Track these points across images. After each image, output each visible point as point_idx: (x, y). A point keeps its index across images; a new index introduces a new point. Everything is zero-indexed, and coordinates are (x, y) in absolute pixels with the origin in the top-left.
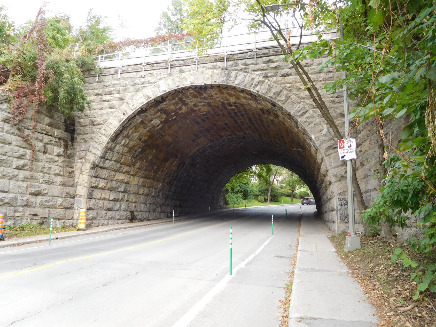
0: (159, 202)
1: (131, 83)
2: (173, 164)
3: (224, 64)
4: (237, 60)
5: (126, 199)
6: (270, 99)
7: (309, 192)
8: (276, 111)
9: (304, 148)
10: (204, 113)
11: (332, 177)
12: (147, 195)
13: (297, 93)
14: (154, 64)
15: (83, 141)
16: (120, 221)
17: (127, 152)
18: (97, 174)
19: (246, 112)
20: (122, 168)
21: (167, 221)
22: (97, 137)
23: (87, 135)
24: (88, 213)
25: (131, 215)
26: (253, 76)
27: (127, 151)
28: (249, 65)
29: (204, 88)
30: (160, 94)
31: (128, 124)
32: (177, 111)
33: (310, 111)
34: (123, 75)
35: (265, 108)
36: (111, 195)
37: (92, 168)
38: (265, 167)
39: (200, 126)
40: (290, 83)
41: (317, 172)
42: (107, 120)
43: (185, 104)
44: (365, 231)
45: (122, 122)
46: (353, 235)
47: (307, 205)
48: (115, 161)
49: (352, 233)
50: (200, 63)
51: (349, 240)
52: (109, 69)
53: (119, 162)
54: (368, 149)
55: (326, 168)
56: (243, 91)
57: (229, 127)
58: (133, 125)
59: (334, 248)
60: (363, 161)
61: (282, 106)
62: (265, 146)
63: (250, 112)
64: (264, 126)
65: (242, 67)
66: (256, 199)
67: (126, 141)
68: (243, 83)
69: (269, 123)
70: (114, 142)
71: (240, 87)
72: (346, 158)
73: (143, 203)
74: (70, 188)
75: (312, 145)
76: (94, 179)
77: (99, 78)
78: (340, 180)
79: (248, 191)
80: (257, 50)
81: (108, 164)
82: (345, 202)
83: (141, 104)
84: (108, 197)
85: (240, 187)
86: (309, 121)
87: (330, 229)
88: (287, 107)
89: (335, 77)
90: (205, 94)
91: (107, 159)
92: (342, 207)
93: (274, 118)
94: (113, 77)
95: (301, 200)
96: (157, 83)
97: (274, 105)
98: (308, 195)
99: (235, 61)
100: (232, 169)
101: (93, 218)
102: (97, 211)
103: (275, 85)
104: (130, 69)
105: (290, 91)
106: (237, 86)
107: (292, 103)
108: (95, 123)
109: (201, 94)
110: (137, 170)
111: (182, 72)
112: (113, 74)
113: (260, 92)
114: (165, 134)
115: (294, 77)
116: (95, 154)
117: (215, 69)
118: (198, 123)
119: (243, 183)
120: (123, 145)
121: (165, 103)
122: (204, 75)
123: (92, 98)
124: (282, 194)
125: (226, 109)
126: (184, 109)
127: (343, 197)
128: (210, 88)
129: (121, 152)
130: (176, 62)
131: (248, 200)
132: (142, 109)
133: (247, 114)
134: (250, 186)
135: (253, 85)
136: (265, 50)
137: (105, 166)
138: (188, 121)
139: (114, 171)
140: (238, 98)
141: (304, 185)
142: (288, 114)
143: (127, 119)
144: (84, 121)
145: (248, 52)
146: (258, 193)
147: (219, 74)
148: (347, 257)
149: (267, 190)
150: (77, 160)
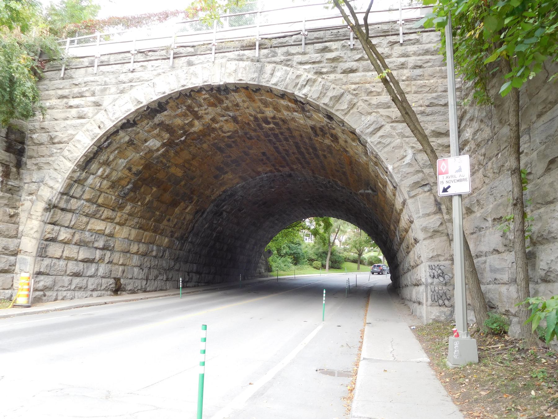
0: (164, 265)
1: (114, 81)
2: (187, 211)
3: (255, 53)
5: (107, 260)
6: (324, 107)
7: (381, 257)
8: (334, 129)
9: (375, 189)
10: (229, 134)
12: (145, 255)
13: (367, 98)
14: (150, 51)
15: (36, 167)
16: (95, 294)
17: (108, 188)
18: (55, 220)
19: (291, 133)
20: (101, 213)
21: (172, 293)
22: (56, 162)
23: (42, 158)
24: (38, 280)
25: (116, 284)
26: (299, 73)
27: (108, 186)
28: (293, 54)
29: (224, 90)
30: (155, 98)
31: (106, 143)
32: (187, 127)
33: (386, 126)
34: (102, 68)
35: (318, 125)
37: (47, 210)
38: (323, 221)
39: (224, 155)
40: (355, 84)
41: (394, 226)
42: (74, 135)
43: (197, 117)
44: (478, 323)
45: (96, 139)
46: (464, 336)
47: (379, 274)
48: (88, 200)
49: (461, 332)
50: (219, 51)
51: (456, 345)
52: (79, 60)
53: (95, 203)
54: (480, 186)
55: (410, 217)
56: (283, 95)
57: (268, 159)
58: (115, 145)
59: (425, 355)
60: (471, 205)
61: (342, 118)
62: (321, 189)
63: (296, 134)
64: (317, 156)
65: (283, 58)
66: (311, 265)
67: (104, 170)
68: (283, 83)
69: (324, 151)
70: (83, 170)
71: (279, 88)
72: (450, 192)
73: (137, 266)
74: (10, 240)
75: (388, 181)
76: (51, 227)
77: (66, 72)
78: (431, 237)
79: (299, 253)
80: (306, 33)
81: (74, 204)
82: (440, 271)
83: (127, 112)
84: (75, 255)
85: (289, 247)
86: (384, 141)
87: (412, 314)
88: (352, 121)
89: (426, 74)
90: (227, 102)
91: (72, 197)
92: (435, 279)
93: (332, 141)
94: (86, 72)
95: (370, 268)
96: (152, 81)
97: (330, 117)
98: (380, 261)
99: (273, 49)
100: (276, 222)
101: (46, 288)
102: (54, 277)
104: (112, 59)
105: (356, 95)
106: (274, 87)
107: (358, 115)
108: (56, 140)
109: (221, 102)
110: (125, 216)
111: (190, 64)
112: (87, 67)
113: (309, 96)
114: (170, 164)
115: (363, 73)
116: (52, 188)
117: (242, 60)
118: (221, 150)
119: (293, 243)
120: (101, 177)
121: (165, 113)
122: (223, 69)
123: (54, 102)
124: (345, 259)
125: (261, 128)
126: (198, 126)
127: (436, 263)
128: (233, 91)
129: (97, 188)
130: (181, 50)
132: (128, 121)
133: (293, 137)
134: (303, 246)
135: (299, 86)
136: (318, 33)
137: (69, 208)
138: (205, 146)
139: (87, 215)
140: (276, 108)
141: (374, 247)
142: (351, 132)
143: (104, 135)
144: (40, 138)
145: (292, 36)
147: (248, 68)
148: (453, 379)
149: (325, 253)
150: (24, 196)
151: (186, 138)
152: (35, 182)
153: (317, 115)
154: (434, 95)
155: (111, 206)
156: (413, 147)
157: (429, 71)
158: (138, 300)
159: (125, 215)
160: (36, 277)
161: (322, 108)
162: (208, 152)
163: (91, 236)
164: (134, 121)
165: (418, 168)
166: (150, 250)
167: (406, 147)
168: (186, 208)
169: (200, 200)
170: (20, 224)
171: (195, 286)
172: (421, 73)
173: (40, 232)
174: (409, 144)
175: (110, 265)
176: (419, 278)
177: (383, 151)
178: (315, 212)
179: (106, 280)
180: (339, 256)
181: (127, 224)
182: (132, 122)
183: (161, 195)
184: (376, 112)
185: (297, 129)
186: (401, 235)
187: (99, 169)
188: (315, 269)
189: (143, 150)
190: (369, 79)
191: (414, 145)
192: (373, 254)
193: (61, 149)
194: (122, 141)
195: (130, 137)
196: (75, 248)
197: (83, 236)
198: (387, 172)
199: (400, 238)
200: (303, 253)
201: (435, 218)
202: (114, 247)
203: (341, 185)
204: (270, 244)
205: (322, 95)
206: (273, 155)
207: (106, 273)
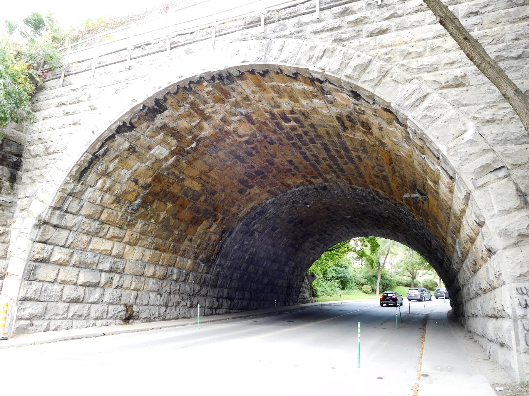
3: (261, 29)
4: (283, 19)
5: (115, 283)
6: (347, 80)
7: (437, 279)
10: (246, 138)
11: (496, 237)
12: (163, 278)
13: (404, 62)
16: (99, 322)
17: (112, 203)
18: (46, 238)
20: (105, 231)
25: (127, 311)
27: (111, 201)
28: (306, 24)
29: (227, 78)
33: (434, 95)
35: (344, 113)
36: (81, 275)
37: (38, 226)
38: (369, 241)
39: (246, 165)
41: (452, 237)
43: (207, 118)
48: (88, 217)
50: (220, 34)
53: (98, 219)
56: (296, 76)
57: (296, 168)
58: (112, 154)
61: (371, 90)
62: (362, 204)
63: (322, 131)
65: (293, 30)
66: (360, 289)
67: (104, 182)
69: (357, 150)
70: (79, 180)
77: (66, 78)
78: (516, 244)
79: (346, 277)
81: (70, 220)
85: (336, 271)
89: (486, 22)
93: (365, 133)
99: (281, 22)
100: (317, 243)
101: (32, 317)
103: (358, 53)
107: (393, 84)
108: (50, 151)
109: (227, 95)
113: (326, 70)
114: (184, 176)
115: (396, 33)
120: (101, 189)
121: (166, 113)
124: (397, 282)
125: (282, 129)
126: (208, 130)
129: (98, 202)
131: (346, 291)
133: (319, 136)
134: (350, 270)
135: (314, 59)
137: (63, 224)
138: (221, 154)
139: (87, 233)
143: (98, 140)
146: (363, 281)
149: (375, 277)
150: (18, 213)
151: (197, 145)
152: (28, 197)
153: (339, 96)
154: (501, 46)
155: (118, 224)
156: (475, 118)
157: (492, 16)
158: (148, 330)
159: (135, 234)
160: (21, 303)
161: (345, 82)
162: (226, 161)
163: (95, 257)
164: (130, 123)
165: (485, 146)
166: (169, 273)
167: (463, 118)
168: (210, 227)
169: (226, 218)
170: (11, 243)
171: (226, 313)
172: (479, 21)
173: (28, 252)
174: (468, 114)
175: (119, 290)
176: (500, 308)
177: (430, 128)
178: (359, 231)
179: (114, 306)
180: (391, 280)
181: (139, 244)
182: (128, 125)
183: (178, 212)
184: (417, 78)
185: (322, 124)
186: (464, 248)
187: (97, 181)
188: (365, 294)
189: (148, 160)
190: (405, 39)
191: (476, 115)
192: (427, 278)
193: (55, 158)
194: (121, 148)
195: (130, 143)
196: (74, 271)
197: (83, 256)
198: (438, 158)
199: (462, 253)
200: (351, 277)
201: (519, 216)
202: (124, 269)
203: (383, 195)
204: (311, 268)
205: (343, 66)
206: (301, 163)
207: (114, 299)
